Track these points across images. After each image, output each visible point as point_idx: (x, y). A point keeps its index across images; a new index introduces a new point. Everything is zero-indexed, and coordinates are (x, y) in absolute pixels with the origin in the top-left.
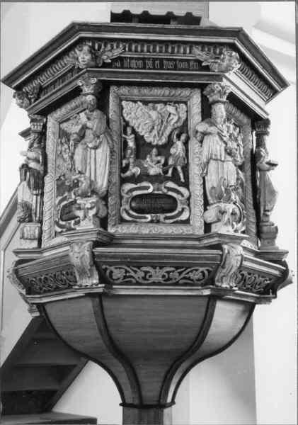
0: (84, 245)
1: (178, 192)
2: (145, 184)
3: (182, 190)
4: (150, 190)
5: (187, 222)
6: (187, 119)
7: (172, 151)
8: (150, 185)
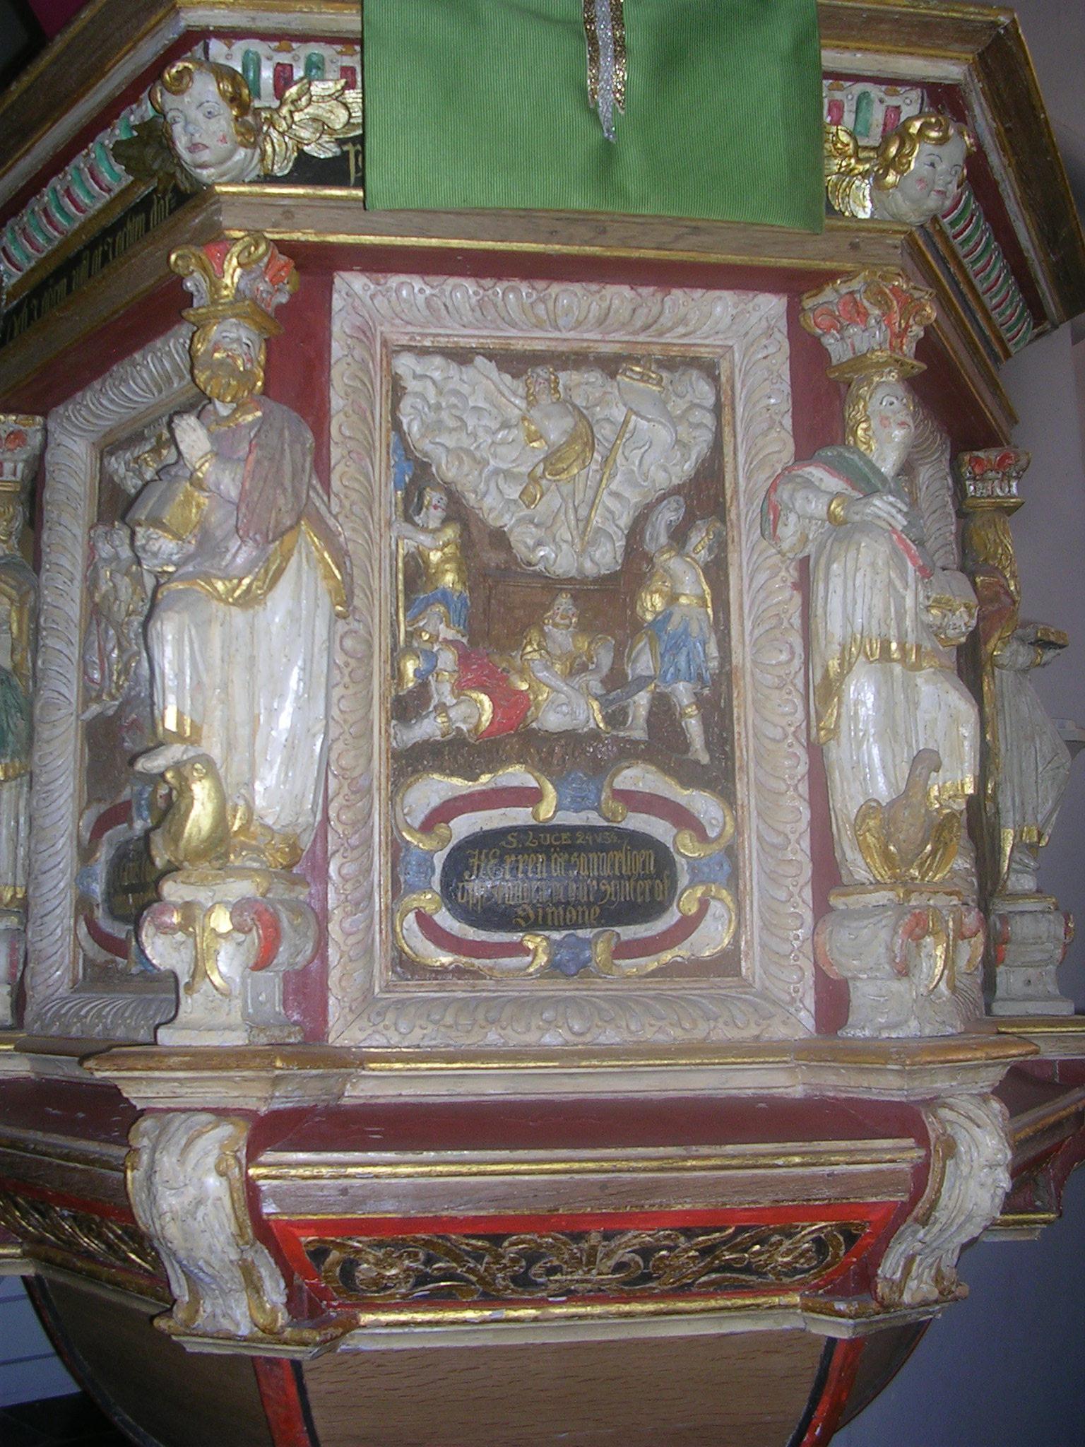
0: (201, 1143)
1: (681, 817)
2: (517, 775)
3: (703, 804)
4: (547, 810)
5: (727, 963)
6: (717, 446)
7: (653, 603)
8: (550, 789)
